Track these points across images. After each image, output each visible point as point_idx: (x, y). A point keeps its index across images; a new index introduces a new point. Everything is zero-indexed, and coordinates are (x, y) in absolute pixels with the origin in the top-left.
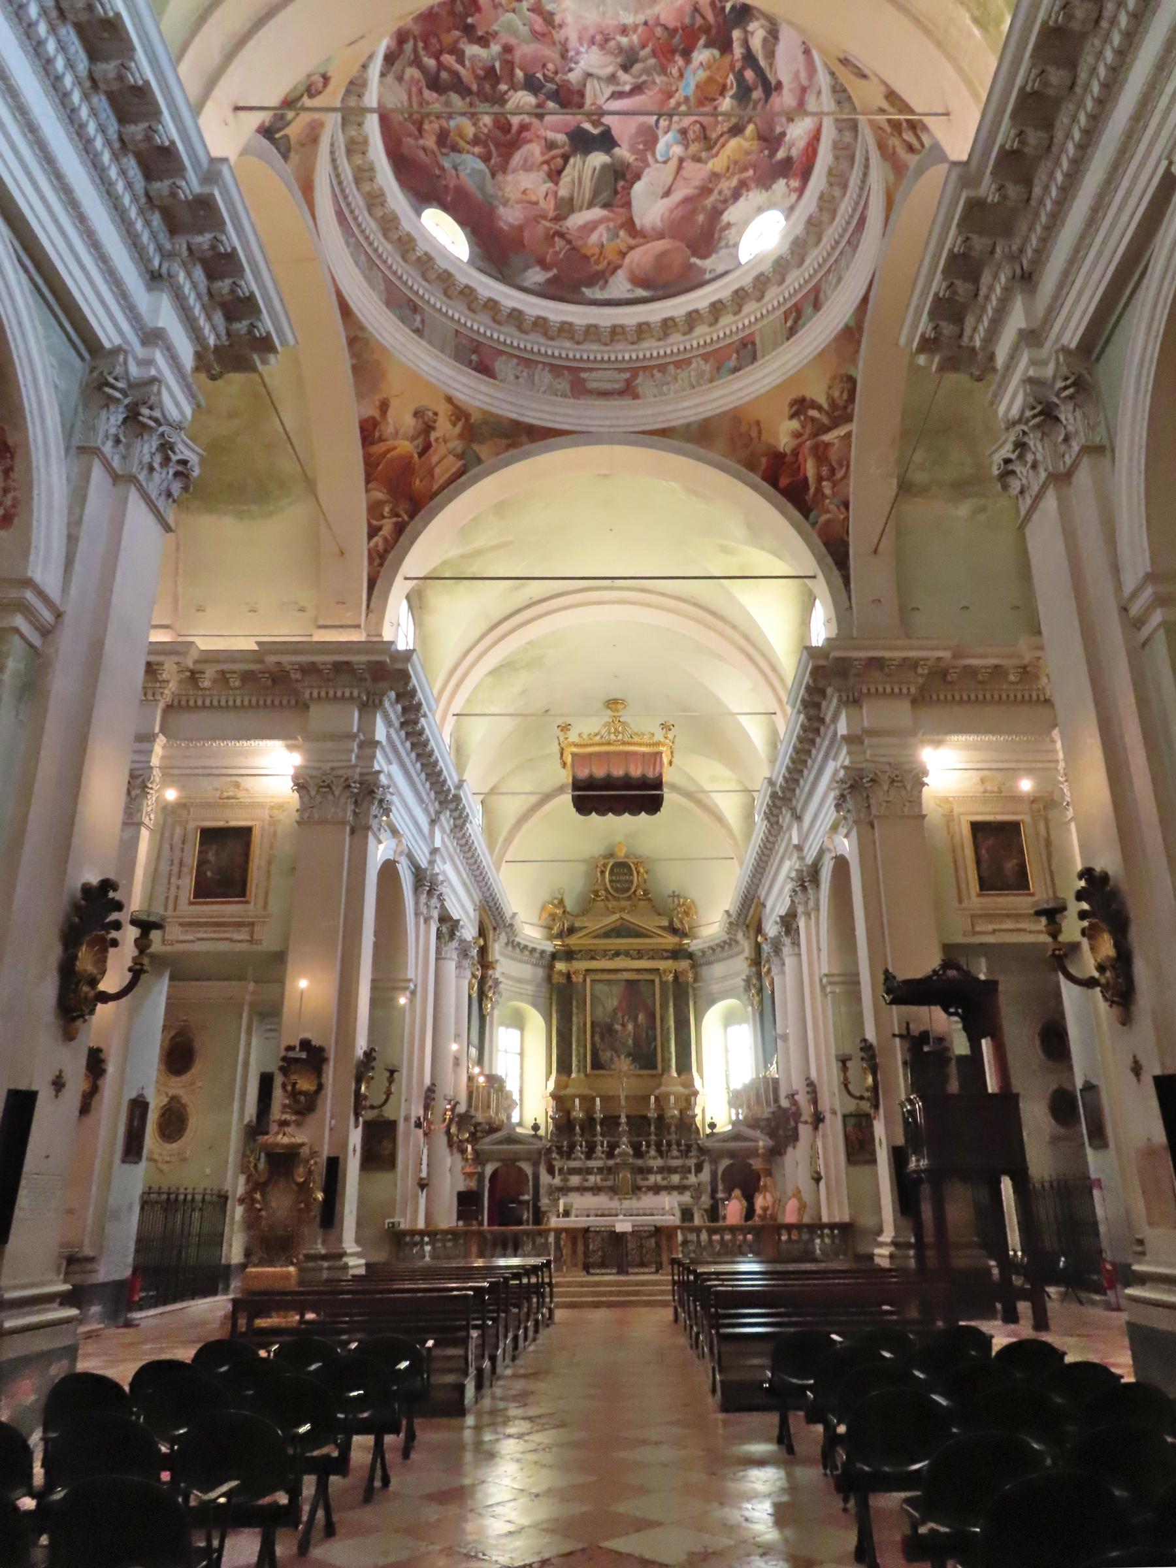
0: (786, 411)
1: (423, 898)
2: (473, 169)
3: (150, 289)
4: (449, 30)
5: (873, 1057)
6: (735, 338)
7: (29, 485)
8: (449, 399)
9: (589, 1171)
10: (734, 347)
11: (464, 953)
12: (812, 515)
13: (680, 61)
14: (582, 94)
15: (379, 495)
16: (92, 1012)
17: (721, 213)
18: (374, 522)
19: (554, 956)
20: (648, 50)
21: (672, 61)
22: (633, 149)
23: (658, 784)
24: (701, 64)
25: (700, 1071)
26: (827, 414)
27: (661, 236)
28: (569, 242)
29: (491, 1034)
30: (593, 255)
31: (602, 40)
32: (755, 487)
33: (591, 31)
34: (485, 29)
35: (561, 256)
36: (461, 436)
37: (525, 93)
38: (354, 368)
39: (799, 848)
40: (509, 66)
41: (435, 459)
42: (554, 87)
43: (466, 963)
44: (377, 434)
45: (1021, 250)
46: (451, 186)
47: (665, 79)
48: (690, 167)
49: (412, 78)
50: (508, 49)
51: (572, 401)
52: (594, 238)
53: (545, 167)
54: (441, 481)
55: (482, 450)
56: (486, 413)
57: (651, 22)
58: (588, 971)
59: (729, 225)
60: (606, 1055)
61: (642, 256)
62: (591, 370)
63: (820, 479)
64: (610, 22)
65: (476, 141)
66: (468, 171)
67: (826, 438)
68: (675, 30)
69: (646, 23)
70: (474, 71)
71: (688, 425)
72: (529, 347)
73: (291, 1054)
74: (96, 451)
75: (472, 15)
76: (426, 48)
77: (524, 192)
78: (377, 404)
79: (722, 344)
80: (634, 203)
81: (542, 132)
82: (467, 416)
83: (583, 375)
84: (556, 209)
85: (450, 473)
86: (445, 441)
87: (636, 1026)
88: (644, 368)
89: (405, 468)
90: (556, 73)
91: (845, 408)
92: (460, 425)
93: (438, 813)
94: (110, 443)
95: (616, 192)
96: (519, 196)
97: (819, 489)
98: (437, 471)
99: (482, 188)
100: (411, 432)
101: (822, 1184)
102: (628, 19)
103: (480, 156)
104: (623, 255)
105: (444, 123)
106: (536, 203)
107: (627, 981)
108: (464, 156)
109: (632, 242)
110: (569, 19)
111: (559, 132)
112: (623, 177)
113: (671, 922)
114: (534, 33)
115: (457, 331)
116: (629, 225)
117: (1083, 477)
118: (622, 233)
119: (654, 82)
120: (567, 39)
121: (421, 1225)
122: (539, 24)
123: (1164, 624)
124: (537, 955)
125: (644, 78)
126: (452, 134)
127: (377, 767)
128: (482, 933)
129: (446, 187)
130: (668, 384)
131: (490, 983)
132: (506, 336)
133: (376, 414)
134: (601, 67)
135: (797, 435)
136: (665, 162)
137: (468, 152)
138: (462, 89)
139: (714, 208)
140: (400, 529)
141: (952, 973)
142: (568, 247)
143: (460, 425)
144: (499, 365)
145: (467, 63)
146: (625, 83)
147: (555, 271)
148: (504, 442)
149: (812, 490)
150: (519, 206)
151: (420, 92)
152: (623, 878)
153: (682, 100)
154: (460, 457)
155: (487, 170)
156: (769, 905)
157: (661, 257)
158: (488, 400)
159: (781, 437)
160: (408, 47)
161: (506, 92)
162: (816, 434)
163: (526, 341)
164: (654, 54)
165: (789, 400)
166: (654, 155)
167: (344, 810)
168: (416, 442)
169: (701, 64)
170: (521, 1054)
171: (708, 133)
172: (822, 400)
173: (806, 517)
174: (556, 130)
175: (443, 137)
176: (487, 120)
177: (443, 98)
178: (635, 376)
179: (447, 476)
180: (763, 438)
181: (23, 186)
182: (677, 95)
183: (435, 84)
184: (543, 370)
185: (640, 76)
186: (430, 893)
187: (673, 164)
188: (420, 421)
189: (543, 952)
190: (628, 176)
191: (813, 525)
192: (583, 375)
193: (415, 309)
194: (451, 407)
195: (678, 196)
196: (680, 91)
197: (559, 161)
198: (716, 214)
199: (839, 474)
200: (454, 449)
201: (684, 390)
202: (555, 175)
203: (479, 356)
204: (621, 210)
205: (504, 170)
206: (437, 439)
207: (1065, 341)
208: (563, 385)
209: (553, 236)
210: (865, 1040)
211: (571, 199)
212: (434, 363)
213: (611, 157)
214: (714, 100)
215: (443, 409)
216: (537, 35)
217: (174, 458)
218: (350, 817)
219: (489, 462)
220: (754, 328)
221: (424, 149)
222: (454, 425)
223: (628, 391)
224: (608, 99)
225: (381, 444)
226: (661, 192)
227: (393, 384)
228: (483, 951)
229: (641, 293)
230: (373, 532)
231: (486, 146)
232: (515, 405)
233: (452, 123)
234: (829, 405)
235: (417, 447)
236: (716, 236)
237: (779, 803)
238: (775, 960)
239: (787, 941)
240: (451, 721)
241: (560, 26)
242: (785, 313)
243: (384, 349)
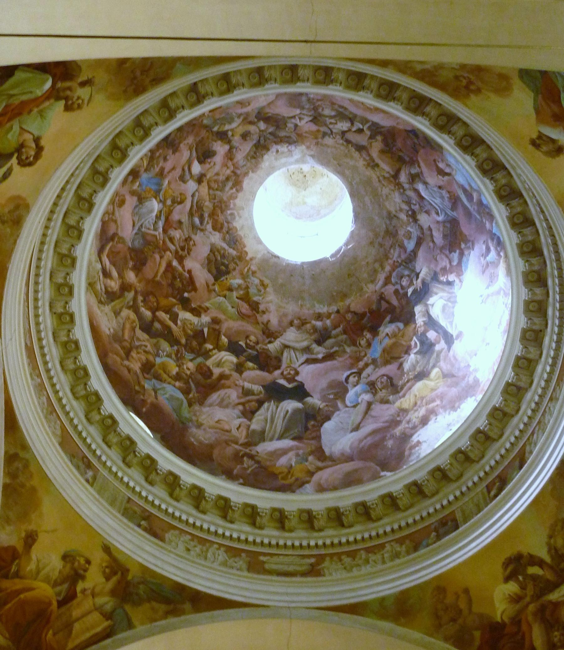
0: (499, 571)
2: (172, 396)
4: (166, 297)
6: (433, 520)
8: (107, 549)
10: (433, 527)
13: (368, 335)
14: (279, 360)
17: (411, 435)
20: (340, 329)
21: (362, 336)
22: (324, 398)
24: (387, 334)
26: (551, 567)
31: (301, 323)
33: (290, 318)
34: (198, 304)
35: (249, 471)
36: (113, 593)
37: (228, 353)
38: (6, 487)
40: (216, 334)
41: (76, 613)
42: (255, 353)
44: (14, 568)
46: (149, 401)
47: (354, 348)
48: (378, 409)
49: (128, 318)
50: (216, 321)
52: (283, 461)
53: (241, 407)
55: (135, 613)
56: (145, 570)
57: (342, 311)
59: (419, 443)
64: (306, 312)
65: (178, 377)
66: (167, 396)
68: (363, 315)
69: (338, 312)
70: (184, 330)
71: (383, 599)
72: (205, 526)
75: (189, 292)
76: (144, 301)
77: (218, 422)
78: (23, 534)
79: (419, 527)
80: (323, 437)
81: (241, 383)
82: (125, 571)
83: (262, 558)
84: (247, 436)
85: (92, 632)
86: (93, 595)
90: (257, 343)
92: (115, 579)
95: (306, 429)
96: (212, 423)
98: (77, 626)
99: (178, 410)
100: (55, 575)
102: (323, 309)
103: (180, 389)
105: (151, 358)
106: (229, 431)
108: (165, 385)
110: (272, 307)
111: (255, 384)
114: (240, 313)
115: (129, 499)
116: (319, 453)
119: (344, 351)
120: (269, 321)
122: (245, 308)
125: (336, 349)
126: (156, 367)
129: (144, 401)
133: (20, 547)
134: (297, 342)
135: (516, 599)
136: (354, 407)
137: (169, 383)
138: (173, 341)
142: (256, 465)
143: (115, 579)
145: (179, 322)
146: (318, 353)
148: (162, 608)
151: (133, 329)
153: (370, 361)
154: (108, 616)
155: (185, 401)
159: (497, 604)
160: (130, 296)
161: (211, 350)
162: (538, 596)
163: (203, 520)
164: (345, 332)
165: (503, 560)
166: (343, 401)
168: (58, 589)
169: (387, 334)
171: (395, 381)
172: (543, 554)
174: (252, 382)
175: (147, 367)
176: (191, 365)
177: (154, 341)
179: (88, 635)
180: (475, 609)
182: (366, 359)
183: (147, 328)
184: (219, 549)
185: (332, 347)
187: (362, 408)
188: (69, 565)
190: (319, 418)
192: (262, 558)
193: (89, 465)
194: (106, 557)
196: (368, 355)
197: (254, 404)
198: (406, 437)
200: (102, 606)
202: (249, 414)
204: (313, 442)
205: (201, 403)
206: (84, 591)
209: (243, 456)
211: (263, 432)
213: (303, 404)
214: (400, 358)
216: (242, 316)
219: (140, 629)
220: (453, 508)
221: (129, 370)
222: (108, 579)
224: (302, 364)
225: (17, 581)
226: (350, 428)
231: (187, 383)
233: (158, 360)
234: (552, 558)
235: (58, 594)
236: (407, 453)
241: (264, 312)
242: (487, 486)
243: (45, 477)
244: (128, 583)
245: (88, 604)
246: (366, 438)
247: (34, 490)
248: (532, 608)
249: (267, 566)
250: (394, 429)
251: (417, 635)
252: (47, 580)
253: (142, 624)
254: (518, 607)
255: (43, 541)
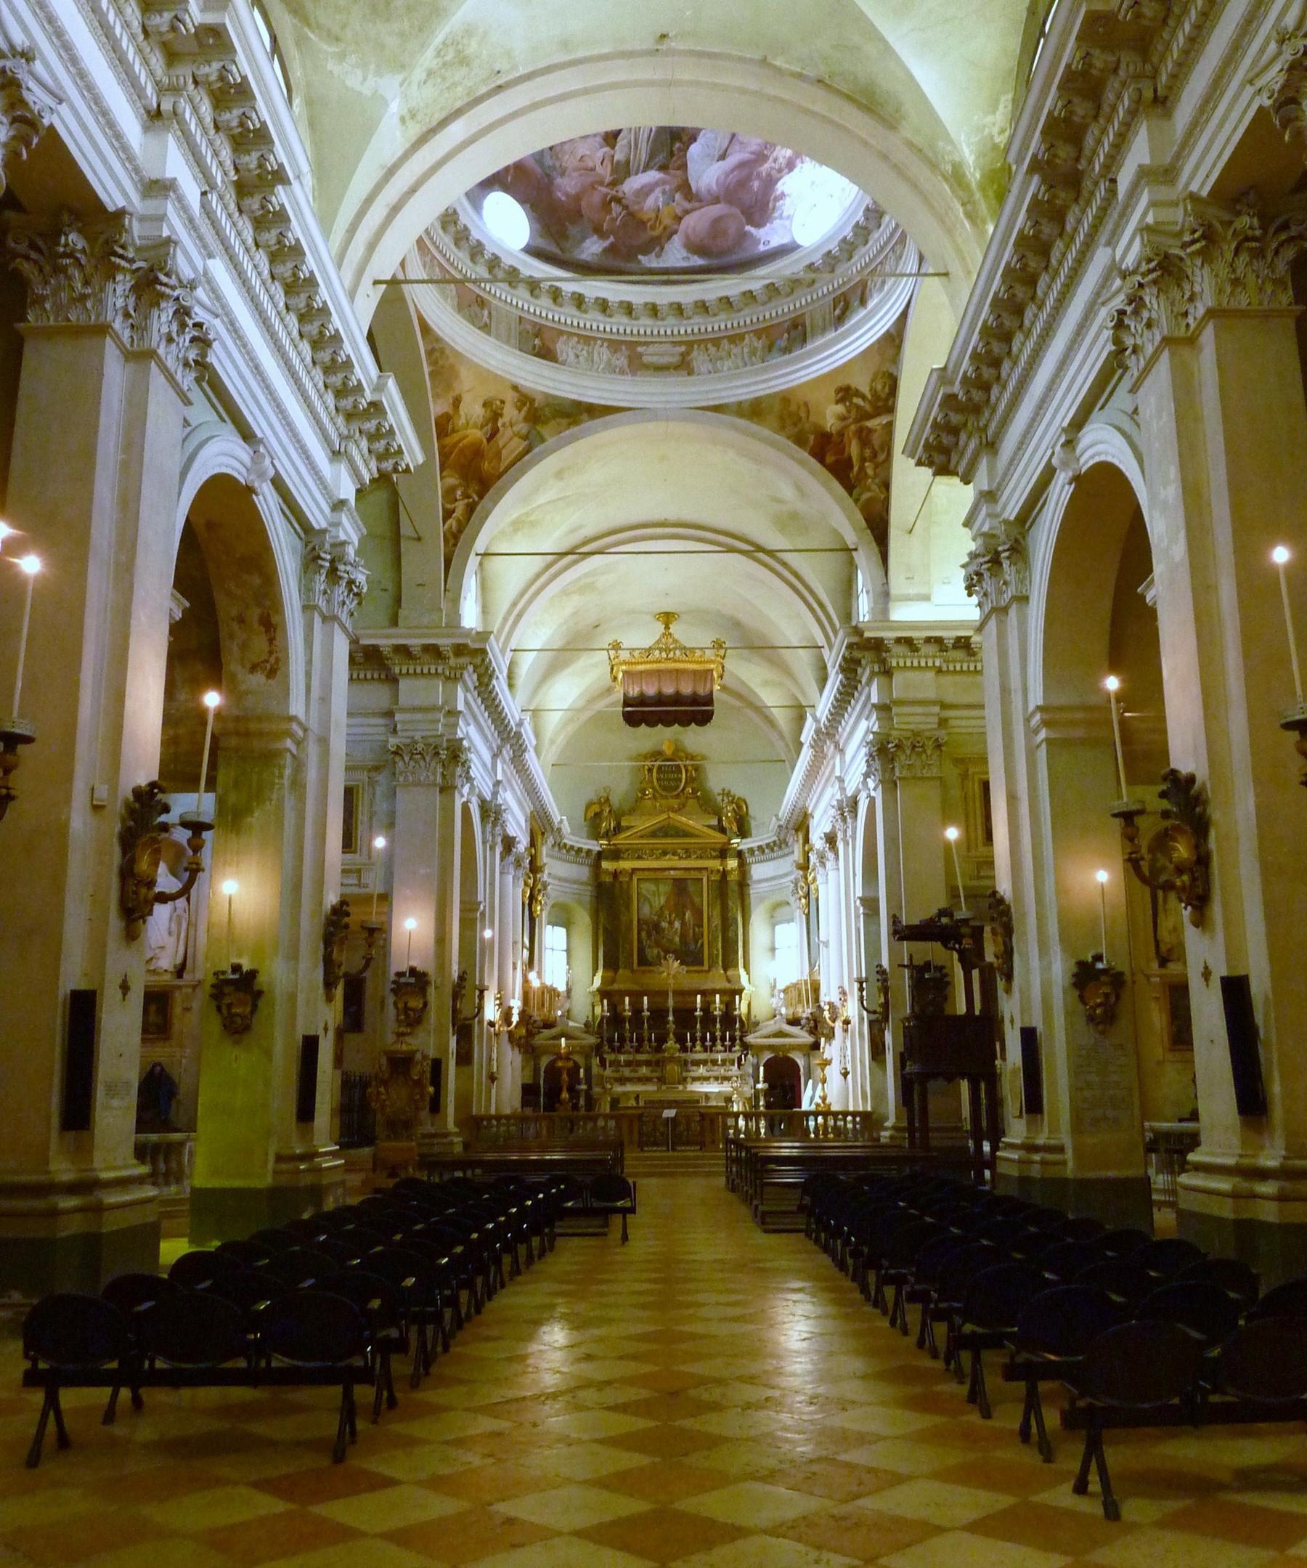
1: (320, 582)
3: (331, 461)
5: (885, 980)
7: (286, 649)
8: (515, 388)
9: (639, 1064)
11: (518, 864)
12: (855, 492)
15: (452, 481)
16: (150, 913)
18: (448, 506)
19: (600, 855)
23: (709, 700)
25: (746, 967)
27: (716, 200)
28: (626, 207)
29: (540, 935)
30: (649, 220)
32: (801, 462)
36: (526, 419)
39: (841, 780)
43: (521, 872)
45: (986, 426)
51: (629, 377)
52: (650, 202)
54: (506, 463)
55: (544, 430)
56: (547, 395)
58: (634, 870)
60: (652, 952)
61: (696, 222)
62: (646, 344)
63: (863, 460)
67: (871, 424)
71: (740, 403)
73: (403, 980)
74: (315, 607)
79: (774, 322)
82: (532, 401)
83: (640, 349)
84: (613, 171)
87: (683, 924)
88: (700, 342)
89: (477, 453)
91: (887, 400)
92: (525, 409)
93: (500, 749)
94: (119, 319)
97: (862, 468)
101: (849, 1077)
104: (679, 219)
106: (593, 169)
107: (675, 880)
109: (687, 205)
112: (680, 139)
113: (720, 820)
117: (1013, 612)
118: (678, 196)
121: (493, 1111)
123: (1047, 740)
124: (583, 854)
127: (460, 735)
128: (533, 844)
130: (721, 359)
131: (539, 886)
132: (566, 316)
135: (843, 418)
139: (769, 175)
140: (471, 509)
141: (944, 920)
143: (525, 409)
144: (562, 347)
147: (612, 239)
148: (565, 421)
149: (856, 469)
150: (575, 174)
152: (672, 776)
154: (525, 438)
156: (817, 815)
157: (717, 221)
158: (550, 384)
162: (858, 420)
167: (434, 774)
170: (568, 951)
172: (865, 390)
173: (851, 494)
178: (688, 353)
180: (812, 419)
181: (75, 134)
186: (495, 824)
189: (589, 851)
190: (685, 139)
191: (856, 501)
192: (640, 349)
194: (516, 395)
195: (732, 160)
198: (771, 182)
199: (881, 457)
201: (738, 368)
203: (542, 340)
204: (679, 172)
207: (1194, 187)
208: (621, 361)
210: (881, 966)
211: (628, 162)
212: (499, 356)
215: (510, 397)
217: (190, 323)
218: (439, 780)
219: (551, 441)
222: (520, 411)
223: (684, 366)
227: (466, 383)
228: (533, 860)
229: (698, 261)
230: (448, 514)
232: (577, 386)
236: (771, 205)
237: (956, 419)
238: (820, 869)
239: (830, 855)
240: (509, 655)
243: (458, 355)
244: (536, 409)
245: (509, 433)
246: (733, 170)
247: (452, 367)
248: (853, 427)
249: (646, 359)
250: (761, 165)
251: (766, 432)
252: (475, 426)
253: (552, 436)
254: (843, 424)
255: (466, 399)
